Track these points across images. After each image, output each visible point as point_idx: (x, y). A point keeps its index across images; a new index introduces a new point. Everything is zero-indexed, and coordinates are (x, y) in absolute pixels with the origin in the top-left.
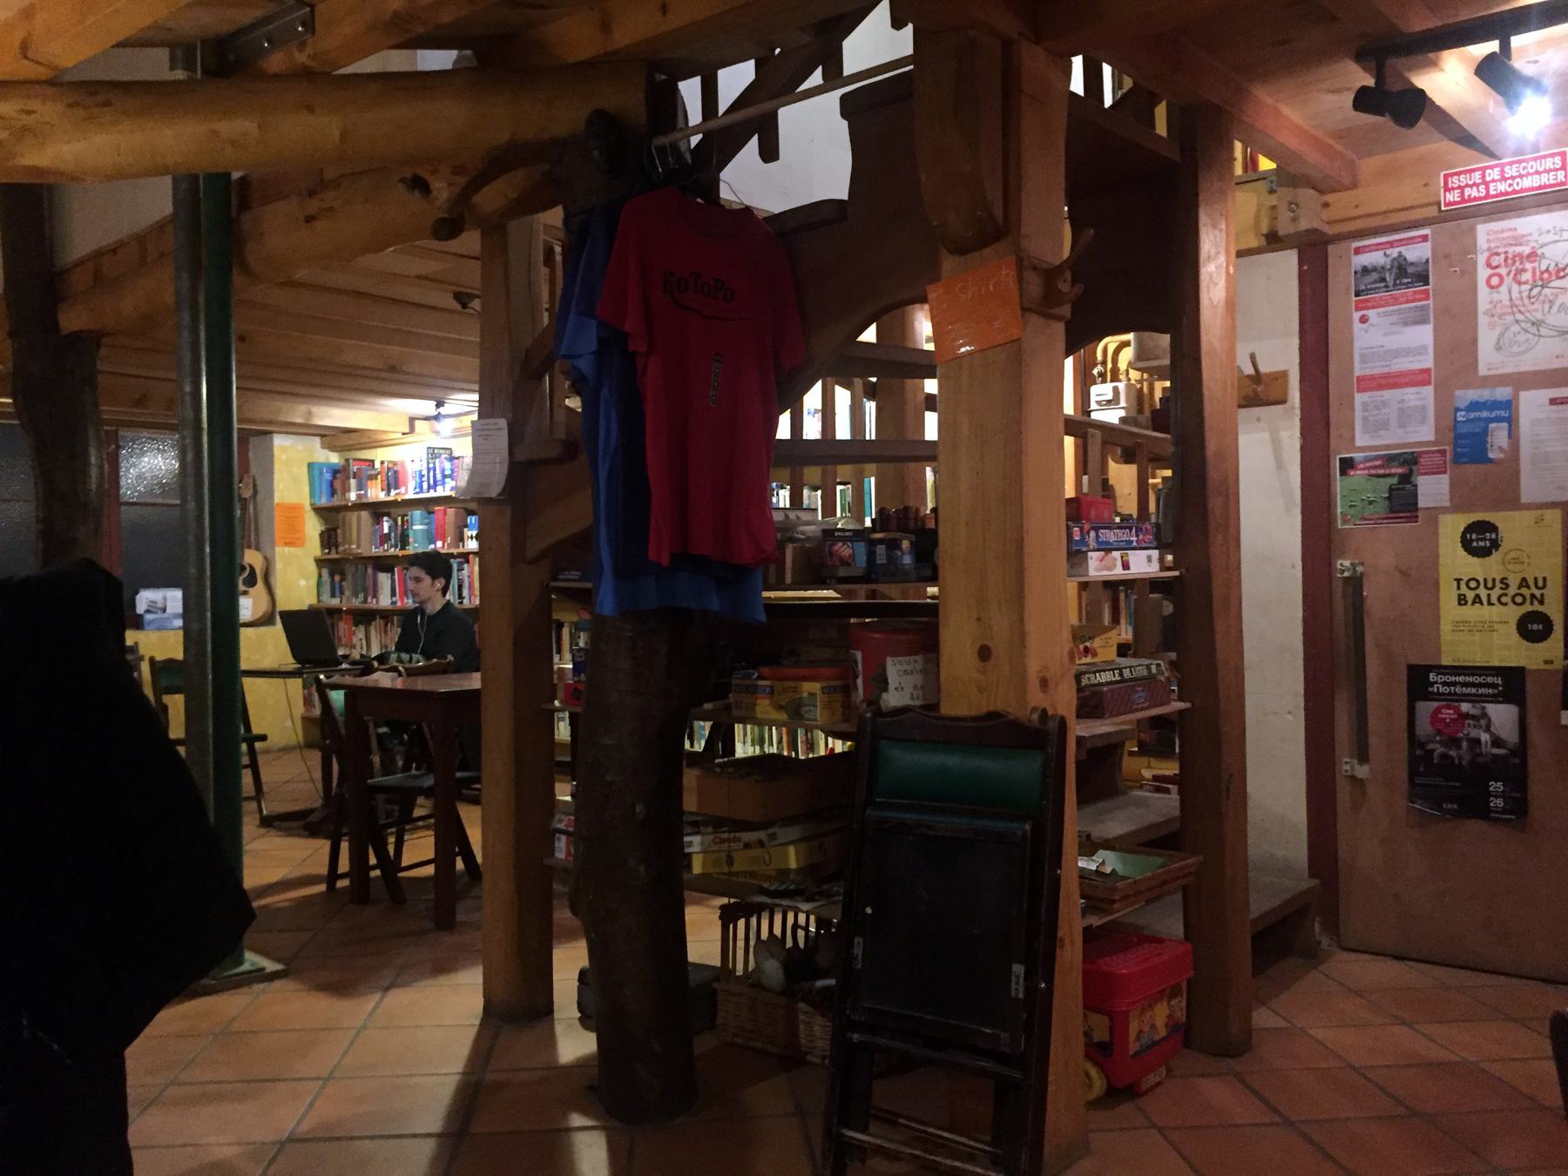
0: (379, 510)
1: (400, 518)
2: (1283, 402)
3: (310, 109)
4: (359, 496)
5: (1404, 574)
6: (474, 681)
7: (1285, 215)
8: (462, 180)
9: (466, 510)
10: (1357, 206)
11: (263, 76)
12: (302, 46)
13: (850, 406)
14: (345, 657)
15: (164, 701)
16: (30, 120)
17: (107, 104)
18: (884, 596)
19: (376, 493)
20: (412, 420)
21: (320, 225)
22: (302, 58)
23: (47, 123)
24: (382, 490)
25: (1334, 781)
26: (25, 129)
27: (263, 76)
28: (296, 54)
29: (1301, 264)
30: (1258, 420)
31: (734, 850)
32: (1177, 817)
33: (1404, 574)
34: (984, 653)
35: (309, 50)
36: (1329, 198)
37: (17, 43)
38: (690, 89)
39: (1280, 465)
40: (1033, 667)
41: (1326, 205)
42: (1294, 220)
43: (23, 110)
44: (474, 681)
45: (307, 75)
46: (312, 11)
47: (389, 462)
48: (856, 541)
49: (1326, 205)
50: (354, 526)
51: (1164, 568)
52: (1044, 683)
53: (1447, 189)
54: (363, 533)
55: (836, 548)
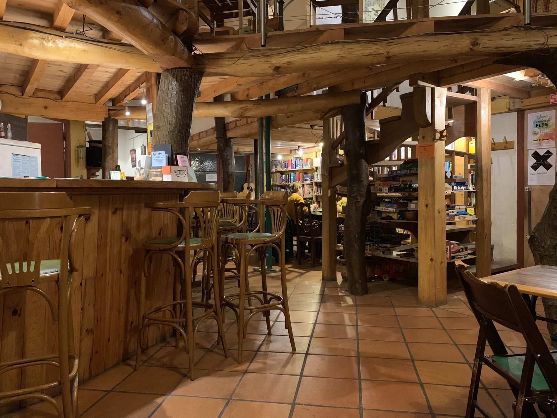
0: (282, 173)
2: (513, 148)
4: (276, 170)
5: (542, 190)
7: (512, 105)
8: (323, 114)
9: (304, 173)
10: (530, 103)
11: (287, 97)
12: (296, 92)
13: (270, 315)
15: (26, 271)
17: (260, 104)
18: (412, 195)
19: (280, 169)
20: (291, 150)
21: (290, 118)
22: (296, 94)
25: (523, 239)
26: (246, 109)
27: (287, 97)
29: (518, 115)
30: (507, 153)
33: (542, 190)
34: (427, 206)
35: (297, 93)
36: (523, 100)
37: (246, 95)
38: (369, 93)
39: (512, 163)
40: (436, 208)
41: (522, 102)
42: (514, 106)
45: (296, 96)
49: (522, 102)
51: (473, 189)
52: (439, 212)
53: (551, 99)
54: (278, 179)
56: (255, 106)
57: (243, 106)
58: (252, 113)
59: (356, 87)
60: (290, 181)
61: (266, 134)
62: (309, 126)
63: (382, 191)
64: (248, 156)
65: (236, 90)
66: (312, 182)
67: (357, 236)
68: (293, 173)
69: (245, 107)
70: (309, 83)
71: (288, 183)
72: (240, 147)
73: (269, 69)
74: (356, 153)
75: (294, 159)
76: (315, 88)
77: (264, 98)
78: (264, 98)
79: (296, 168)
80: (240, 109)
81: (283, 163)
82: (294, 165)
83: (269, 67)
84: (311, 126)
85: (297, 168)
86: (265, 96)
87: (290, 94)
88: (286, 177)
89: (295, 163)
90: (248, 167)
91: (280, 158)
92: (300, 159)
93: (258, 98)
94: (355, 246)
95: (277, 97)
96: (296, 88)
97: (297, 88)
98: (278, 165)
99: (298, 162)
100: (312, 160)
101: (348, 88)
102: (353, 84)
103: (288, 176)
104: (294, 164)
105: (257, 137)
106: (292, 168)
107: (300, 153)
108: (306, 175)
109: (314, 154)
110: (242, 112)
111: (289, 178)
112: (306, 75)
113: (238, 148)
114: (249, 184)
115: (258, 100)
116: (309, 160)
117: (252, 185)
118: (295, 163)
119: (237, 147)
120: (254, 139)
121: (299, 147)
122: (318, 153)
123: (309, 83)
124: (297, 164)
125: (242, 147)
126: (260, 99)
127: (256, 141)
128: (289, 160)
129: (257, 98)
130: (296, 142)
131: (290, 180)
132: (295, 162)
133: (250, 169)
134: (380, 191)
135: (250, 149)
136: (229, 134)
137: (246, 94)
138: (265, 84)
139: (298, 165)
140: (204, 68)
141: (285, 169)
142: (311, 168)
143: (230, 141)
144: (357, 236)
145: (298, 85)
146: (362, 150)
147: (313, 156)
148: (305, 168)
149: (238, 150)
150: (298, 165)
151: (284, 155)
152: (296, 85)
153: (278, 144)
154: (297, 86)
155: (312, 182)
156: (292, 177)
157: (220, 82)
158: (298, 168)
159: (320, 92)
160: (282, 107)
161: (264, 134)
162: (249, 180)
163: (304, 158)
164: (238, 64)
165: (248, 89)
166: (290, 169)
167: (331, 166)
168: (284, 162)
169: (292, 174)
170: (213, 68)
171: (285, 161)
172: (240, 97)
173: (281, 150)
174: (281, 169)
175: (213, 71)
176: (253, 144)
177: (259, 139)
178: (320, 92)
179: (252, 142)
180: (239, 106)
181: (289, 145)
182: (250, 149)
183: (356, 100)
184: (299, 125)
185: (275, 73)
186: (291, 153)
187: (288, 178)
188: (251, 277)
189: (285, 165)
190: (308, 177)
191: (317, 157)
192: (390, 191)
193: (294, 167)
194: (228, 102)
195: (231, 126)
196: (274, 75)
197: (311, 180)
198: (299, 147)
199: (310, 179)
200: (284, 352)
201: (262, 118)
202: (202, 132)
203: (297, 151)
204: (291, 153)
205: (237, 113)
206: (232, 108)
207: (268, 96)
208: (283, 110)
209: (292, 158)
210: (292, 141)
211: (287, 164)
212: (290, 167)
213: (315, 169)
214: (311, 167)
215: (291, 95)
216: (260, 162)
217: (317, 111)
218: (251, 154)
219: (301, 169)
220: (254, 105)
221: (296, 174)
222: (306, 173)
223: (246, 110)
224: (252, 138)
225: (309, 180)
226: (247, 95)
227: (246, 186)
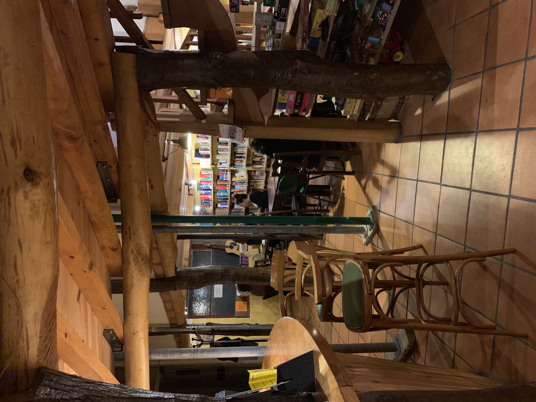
1: (219, 200)
3: (130, 166)
6: (251, 35)
8: (150, 123)
12: (110, 167)
14: (252, 213)
16: (135, 251)
17: (129, 229)
20: (189, 194)
22: (114, 167)
23: (136, 246)
24: (210, 207)
28: (113, 169)
31: (420, 296)
32: (166, 209)
35: (112, 164)
43: (132, 253)
44: (251, 35)
45: (118, 167)
46: (100, 162)
47: (201, 205)
48: (426, 94)
50: (219, 214)
55: (366, 47)
56: (132, 238)
57: (131, 258)
58: (143, 242)
59: (105, 58)
60: (225, 198)
61: (175, 222)
62: (164, 164)
63: (281, 34)
64: (193, 247)
65: (105, 270)
66: (229, 170)
67: (356, 74)
68: (216, 193)
69: (133, 255)
70: (95, 141)
71: (228, 199)
72: (184, 257)
73: (31, 196)
74: (220, 67)
75: (200, 191)
76: (104, 129)
77: (120, 224)
78: (120, 224)
79: (211, 190)
80: (137, 263)
81: (203, 205)
82: (207, 191)
83: (26, 197)
84: (164, 161)
85: (210, 188)
86: (115, 221)
87: (115, 177)
88: (221, 202)
89: (205, 190)
90: (206, 247)
91: (198, 208)
92: (200, 184)
93: (118, 232)
94: (372, 78)
95: (119, 200)
96: (103, 165)
97: (104, 163)
98: (205, 211)
99: (204, 186)
100: (203, 169)
101: (107, 72)
102: (101, 64)
103: (219, 199)
104: (205, 191)
105: (175, 235)
106: (211, 195)
107: (194, 183)
108: (221, 178)
109: (195, 167)
110: (142, 260)
111: (222, 198)
112: (74, 133)
113: (185, 259)
114: (227, 247)
115: (122, 232)
116: (202, 173)
117: (229, 242)
118: (205, 190)
119: (183, 260)
120: (178, 239)
121: (186, 184)
122: (194, 162)
123: (95, 141)
124: (207, 188)
125: (184, 254)
126: (122, 229)
127: (180, 237)
128: (201, 198)
129: (120, 235)
130: (182, 186)
131: (224, 198)
132: (203, 190)
133: (209, 245)
134: (280, 38)
135: (187, 244)
136: (171, 273)
137: (110, 252)
138: (94, 219)
139: (207, 187)
140: (26, 371)
141: (212, 203)
142: (212, 171)
143: (180, 272)
144: (356, 74)
145: (98, 162)
146: (216, 56)
147: (198, 168)
148: (211, 179)
149: (187, 260)
150: (207, 187)
151: (195, 204)
152: (97, 165)
153: (182, 210)
154: (100, 164)
155: (229, 170)
156: (222, 194)
157: (86, 299)
158: (211, 187)
159: (114, 135)
160: (136, 192)
161: (174, 225)
162: (222, 246)
163: (200, 179)
164: (17, 281)
165: (103, 248)
166: (211, 197)
167: (233, 121)
168: (202, 204)
169: (218, 194)
170: (28, 348)
171: (202, 202)
172: (116, 261)
173: (189, 207)
174: (211, 208)
175: (36, 347)
176: (181, 240)
177: (177, 232)
178: (114, 135)
179: (179, 241)
180: (132, 263)
181: (184, 196)
182: (187, 244)
183: (128, 60)
184: (164, 170)
185: (43, 182)
186: (192, 195)
187: (222, 199)
188: (324, 246)
189: (205, 202)
190: (223, 175)
191: (199, 164)
192: (285, 20)
193: (209, 191)
194: (114, 364)
195: (159, 270)
196: (50, 185)
197: (227, 171)
198: (186, 184)
199: (226, 173)
200: (438, 206)
201: (154, 227)
202: (165, 307)
203: (190, 187)
204: (192, 195)
205: (143, 267)
206: (135, 276)
207: (116, 218)
208: (141, 191)
209: (198, 194)
210: (181, 190)
211: (205, 200)
212: (209, 196)
213: (213, 166)
214: (211, 171)
215: (117, 177)
216: (201, 232)
217: (145, 133)
218: (191, 242)
219: (212, 183)
220: (130, 239)
221: (217, 190)
222: (218, 177)
223: (139, 252)
224: (176, 241)
225: (227, 174)
226: (114, 250)
227: (228, 250)
